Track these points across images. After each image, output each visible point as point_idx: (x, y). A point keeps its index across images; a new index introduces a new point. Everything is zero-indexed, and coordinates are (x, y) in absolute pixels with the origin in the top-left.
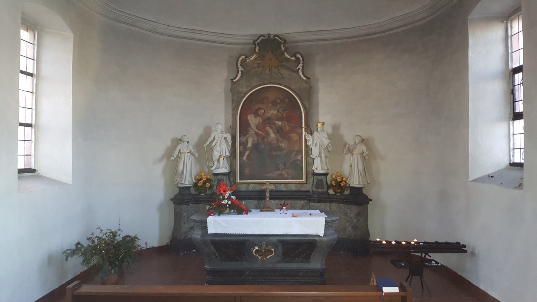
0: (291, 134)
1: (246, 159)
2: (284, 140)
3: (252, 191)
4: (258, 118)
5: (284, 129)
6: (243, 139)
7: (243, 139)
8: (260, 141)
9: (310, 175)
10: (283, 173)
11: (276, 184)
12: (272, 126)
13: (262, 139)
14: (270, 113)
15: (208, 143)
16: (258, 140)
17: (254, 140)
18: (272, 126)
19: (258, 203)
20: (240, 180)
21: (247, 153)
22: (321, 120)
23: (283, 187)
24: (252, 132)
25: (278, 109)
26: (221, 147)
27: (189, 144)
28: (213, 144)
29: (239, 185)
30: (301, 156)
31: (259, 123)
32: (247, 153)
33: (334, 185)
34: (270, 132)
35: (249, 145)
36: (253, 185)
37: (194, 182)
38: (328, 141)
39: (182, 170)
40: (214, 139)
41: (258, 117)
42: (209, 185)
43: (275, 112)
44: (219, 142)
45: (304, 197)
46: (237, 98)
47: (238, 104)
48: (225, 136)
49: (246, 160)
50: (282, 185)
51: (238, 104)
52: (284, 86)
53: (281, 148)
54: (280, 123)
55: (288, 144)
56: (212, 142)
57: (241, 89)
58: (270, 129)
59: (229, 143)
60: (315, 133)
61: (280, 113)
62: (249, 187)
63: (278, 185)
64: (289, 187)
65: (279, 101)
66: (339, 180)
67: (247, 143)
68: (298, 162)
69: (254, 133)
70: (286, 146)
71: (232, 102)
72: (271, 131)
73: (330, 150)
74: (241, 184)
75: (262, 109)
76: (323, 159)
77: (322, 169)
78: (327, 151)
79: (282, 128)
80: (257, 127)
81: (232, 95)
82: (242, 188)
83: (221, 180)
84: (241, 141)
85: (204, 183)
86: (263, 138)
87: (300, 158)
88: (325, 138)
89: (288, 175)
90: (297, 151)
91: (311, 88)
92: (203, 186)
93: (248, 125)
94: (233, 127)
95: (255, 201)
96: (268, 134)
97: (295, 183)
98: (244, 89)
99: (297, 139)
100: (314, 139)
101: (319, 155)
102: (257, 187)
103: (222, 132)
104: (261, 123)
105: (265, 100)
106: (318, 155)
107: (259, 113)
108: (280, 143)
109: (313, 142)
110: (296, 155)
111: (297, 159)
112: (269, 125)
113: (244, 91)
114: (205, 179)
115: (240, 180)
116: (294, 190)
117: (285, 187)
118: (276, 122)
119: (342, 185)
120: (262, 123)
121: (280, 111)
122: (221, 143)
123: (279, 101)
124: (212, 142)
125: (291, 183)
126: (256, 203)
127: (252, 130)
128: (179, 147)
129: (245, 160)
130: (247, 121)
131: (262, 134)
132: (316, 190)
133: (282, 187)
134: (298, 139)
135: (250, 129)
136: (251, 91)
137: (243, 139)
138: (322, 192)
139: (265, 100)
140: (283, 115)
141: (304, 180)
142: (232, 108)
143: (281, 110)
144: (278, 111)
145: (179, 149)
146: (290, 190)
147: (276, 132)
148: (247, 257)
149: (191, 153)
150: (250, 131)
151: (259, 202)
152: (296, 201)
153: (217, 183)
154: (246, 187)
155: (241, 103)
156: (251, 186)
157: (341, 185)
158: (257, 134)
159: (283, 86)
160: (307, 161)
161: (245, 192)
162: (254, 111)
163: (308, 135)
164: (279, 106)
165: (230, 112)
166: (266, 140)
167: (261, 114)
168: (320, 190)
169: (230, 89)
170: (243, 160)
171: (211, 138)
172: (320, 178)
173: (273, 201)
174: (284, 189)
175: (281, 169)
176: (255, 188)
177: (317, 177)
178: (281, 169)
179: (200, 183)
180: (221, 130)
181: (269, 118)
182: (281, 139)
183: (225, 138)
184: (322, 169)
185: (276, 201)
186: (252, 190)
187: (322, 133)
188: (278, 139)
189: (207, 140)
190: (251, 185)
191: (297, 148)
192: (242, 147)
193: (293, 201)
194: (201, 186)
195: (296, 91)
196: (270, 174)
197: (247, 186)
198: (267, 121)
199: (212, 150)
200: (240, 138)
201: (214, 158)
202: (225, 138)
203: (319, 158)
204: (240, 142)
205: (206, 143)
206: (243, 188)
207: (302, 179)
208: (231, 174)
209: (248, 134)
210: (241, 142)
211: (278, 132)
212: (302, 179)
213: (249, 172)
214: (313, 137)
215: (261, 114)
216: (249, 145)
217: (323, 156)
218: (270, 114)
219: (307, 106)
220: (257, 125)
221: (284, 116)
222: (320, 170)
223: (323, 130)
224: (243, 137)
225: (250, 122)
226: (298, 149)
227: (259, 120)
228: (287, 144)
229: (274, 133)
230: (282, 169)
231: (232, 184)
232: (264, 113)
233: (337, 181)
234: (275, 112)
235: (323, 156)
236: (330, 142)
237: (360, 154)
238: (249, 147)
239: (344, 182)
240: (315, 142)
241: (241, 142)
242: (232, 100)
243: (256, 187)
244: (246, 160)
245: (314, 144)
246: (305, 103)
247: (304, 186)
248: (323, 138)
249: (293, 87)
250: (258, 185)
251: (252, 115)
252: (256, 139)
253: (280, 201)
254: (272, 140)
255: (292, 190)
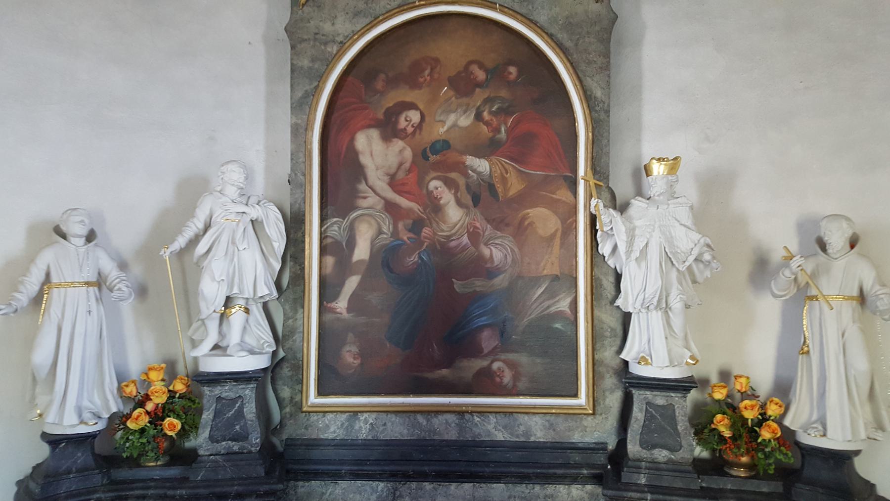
0: (530, 208)
1: (349, 309)
2: (499, 234)
3: (366, 444)
4: (398, 144)
5: (500, 189)
6: (335, 228)
7: (335, 228)
8: (405, 236)
9: (610, 381)
10: (496, 366)
11: (467, 416)
12: (453, 175)
13: (410, 231)
14: (443, 122)
15: (181, 242)
16: (395, 233)
17: (380, 232)
18: (453, 175)
19: (395, 494)
20: (321, 393)
21: (352, 283)
22: (649, 149)
23: (495, 428)
24: (371, 200)
25: (478, 108)
26: (232, 260)
27: (96, 245)
28: (201, 248)
29: (314, 417)
30: (569, 300)
31: (401, 165)
32: (352, 283)
33: (727, 434)
34: (442, 202)
35: (362, 252)
36: (374, 415)
37: (114, 410)
38: (696, 236)
39: (50, 361)
40: (207, 228)
41: (395, 140)
42: (179, 427)
43: (466, 121)
44: (224, 239)
45: (585, 472)
46: (313, 60)
47: (317, 87)
48: (255, 212)
49: (345, 315)
50: (492, 419)
51: (317, 87)
52: (504, 9)
53: (488, 265)
54: (482, 165)
55: (516, 250)
56: (194, 241)
57: (327, 27)
58: (446, 190)
59: (276, 245)
60: (637, 204)
61: (487, 124)
62: (357, 427)
63: (477, 419)
64: (522, 428)
65: (481, 75)
66: (750, 415)
67: (351, 243)
68: (558, 326)
69: (380, 205)
70: (509, 259)
71: (292, 86)
72: (447, 197)
73: (699, 278)
74: (324, 411)
75: (412, 106)
76: (677, 321)
77: (672, 364)
78: (690, 282)
79: (491, 187)
80: (394, 183)
81: (293, 47)
82: (327, 427)
83: (234, 401)
84: (327, 237)
85: (157, 418)
86: (417, 226)
87: (564, 305)
88: (685, 226)
89: (516, 377)
90: (556, 278)
91: (614, 18)
92: (152, 432)
93: (358, 172)
94: (297, 181)
95: (382, 485)
96: (435, 207)
97: (545, 412)
98: (342, 26)
99: (553, 230)
100: (634, 229)
101: (659, 301)
102: (389, 424)
103: (244, 200)
104: (407, 165)
105: (427, 72)
106: (655, 301)
107: (402, 124)
108: (486, 244)
109: (630, 243)
110: (551, 294)
111: (553, 309)
112: (439, 174)
113: (339, 35)
114: (159, 399)
115: (321, 393)
116: (542, 440)
117: (505, 427)
118: (471, 161)
119: (765, 434)
120: (414, 163)
121: (486, 115)
122: (234, 243)
123: (481, 75)
124: (194, 241)
125: (528, 411)
126: (382, 491)
127: (370, 193)
128: (46, 258)
129: (341, 314)
130: (353, 154)
131: (410, 210)
132: (645, 454)
133: (490, 427)
134: (557, 231)
135: (362, 186)
136: (369, 30)
137: (336, 229)
138: (670, 461)
139: (427, 72)
140: (499, 131)
141: (582, 399)
142: (292, 104)
143: (490, 113)
144: (478, 117)
145: (45, 268)
146: (522, 439)
147: (468, 199)
148: (386, 432)
149: (108, 284)
150: (365, 198)
151: (396, 489)
152: (550, 489)
153: (215, 416)
154: (342, 424)
155: (325, 82)
156: (366, 421)
157: (758, 435)
158: (390, 207)
159: (502, 12)
160: (596, 322)
161: (342, 444)
162: (380, 115)
163: (610, 215)
164: (480, 96)
165: (285, 118)
166: (426, 231)
167: (410, 130)
168: (661, 455)
169: (285, 28)
170: (333, 311)
171: (195, 220)
172: (660, 399)
173: (453, 486)
174: (500, 436)
175: (486, 351)
176: (381, 428)
177: (649, 394)
178: (486, 351)
179: (139, 420)
180: (242, 188)
181: (442, 146)
182: (489, 230)
183: (255, 224)
184: (672, 364)
185: (467, 486)
186: (370, 437)
187: (668, 205)
188: (476, 227)
189: (179, 232)
190: (366, 415)
191: (550, 265)
192: (330, 260)
193: (537, 488)
194: (142, 431)
195: (552, 31)
196: (444, 372)
197: (348, 420)
198: (433, 158)
199: (198, 267)
200: (321, 225)
201: (202, 305)
202: (255, 224)
203: (656, 317)
204: (323, 237)
205: (173, 241)
206: (332, 429)
207: (575, 395)
208: (286, 371)
209: (355, 208)
210: (329, 240)
211: (476, 200)
212: (575, 395)
213: (357, 362)
214: (630, 220)
215: (410, 130)
216: (362, 252)
217: (676, 304)
218: (445, 128)
219: (598, 93)
220: (393, 171)
221: (503, 135)
222: (662, 368)
223: (671, 194)
224: (335, 219)
225: (365, 160)
226: (556, 271)
227: (401, 151)
228: (512, 250)
229: (459, 203)
230: (493, 352)
231: (288, 410)
232: (419, 127)
233: (742, 417)
234: (466, 121)
235: (676, 304)
236: (708, 246)
237: (851, 298)
238: (360, 262)
239: (775, 425)
240: (639, 244)
241: (329, 240)
242: (293, 71)
243: (385, 424)
244: (345, 315)
245: (636, 254)
246: (589, 82)
247: (585, 423)
248: (677, 224)
249: (542, 18)
250: (393, 417)
251: (374, 133)
252: (387, 228)
253: (483, 485)
254: (455, 234)
255: (532, 439)
